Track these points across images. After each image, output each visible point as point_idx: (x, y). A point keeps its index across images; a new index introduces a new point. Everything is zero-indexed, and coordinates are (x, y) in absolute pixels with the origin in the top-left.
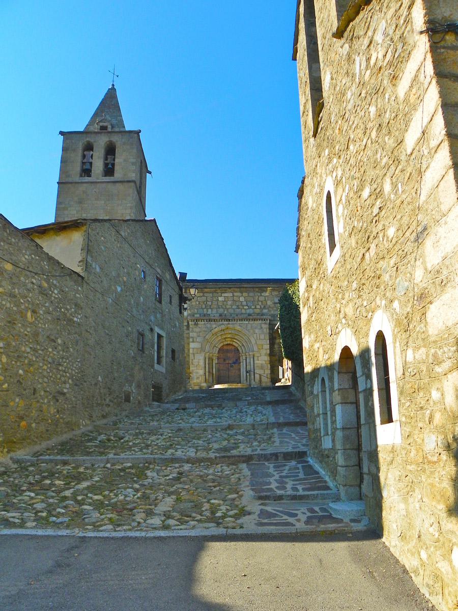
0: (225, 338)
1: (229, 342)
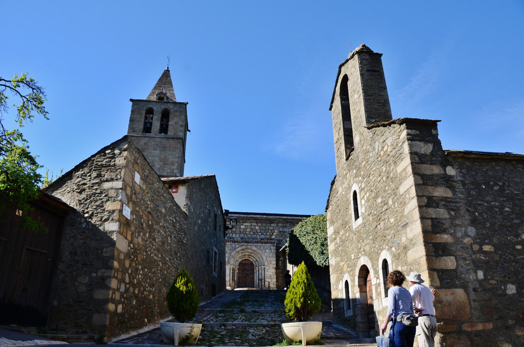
0: (244, 255)
1: (247, 258)
